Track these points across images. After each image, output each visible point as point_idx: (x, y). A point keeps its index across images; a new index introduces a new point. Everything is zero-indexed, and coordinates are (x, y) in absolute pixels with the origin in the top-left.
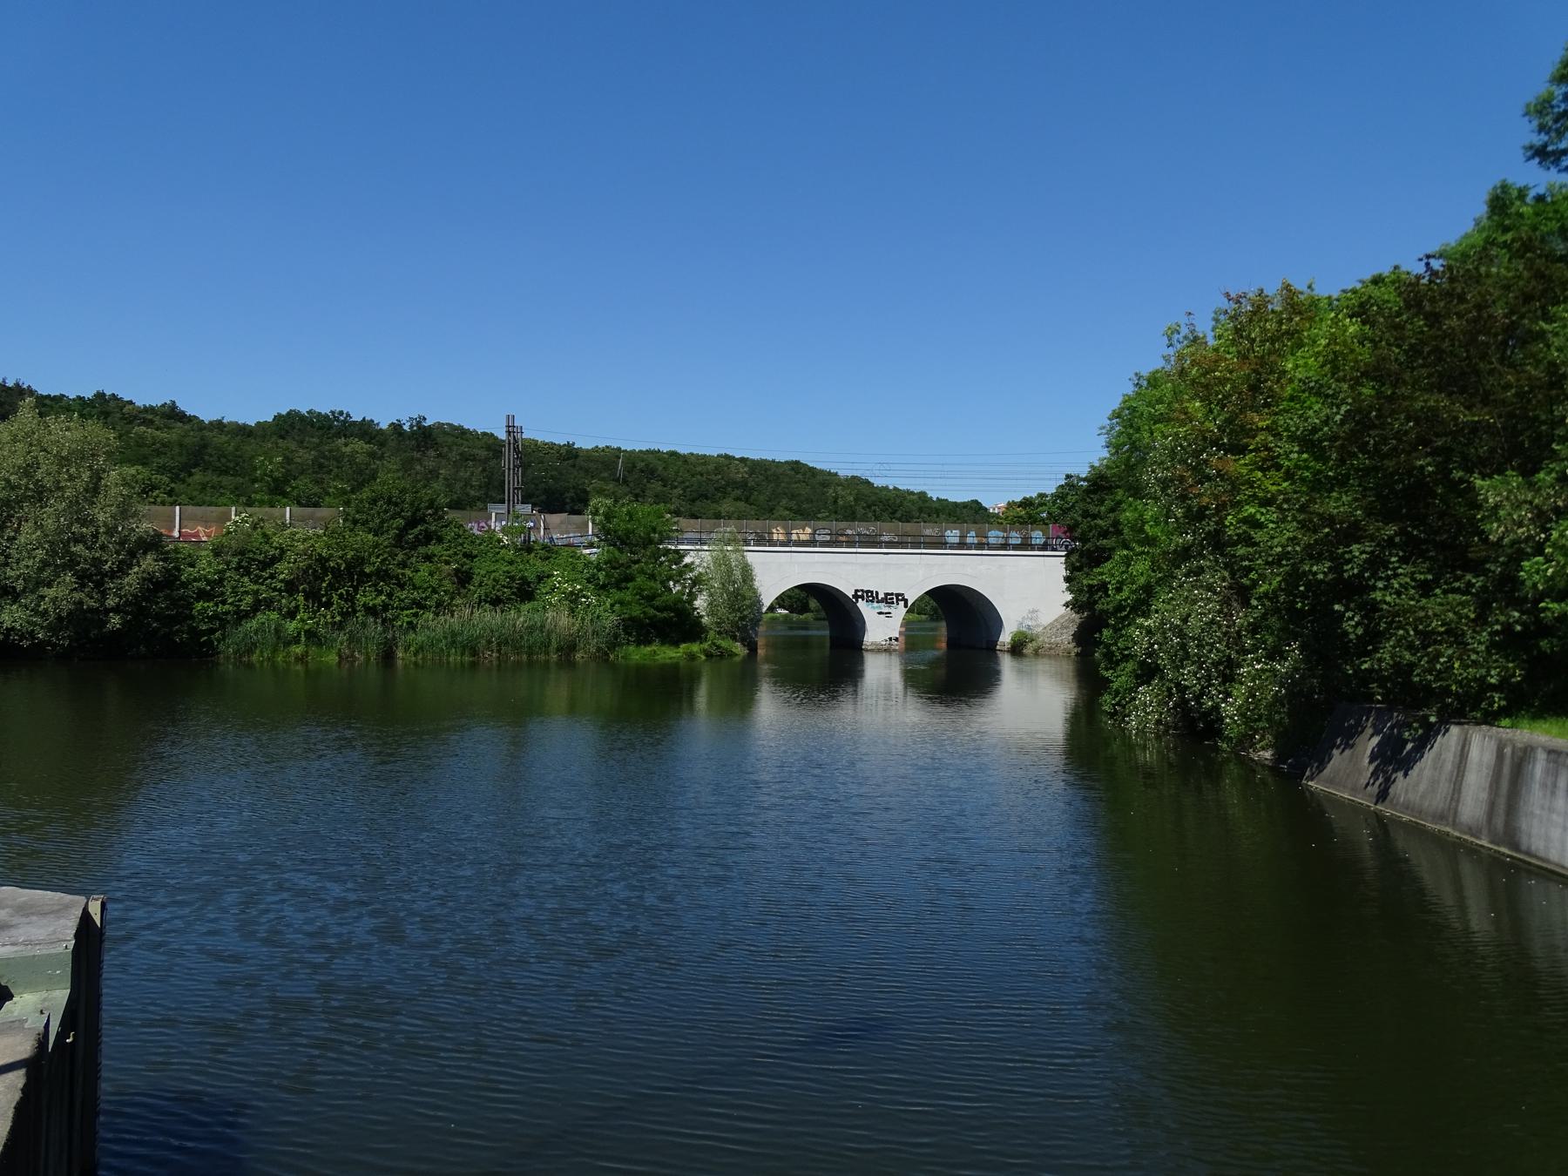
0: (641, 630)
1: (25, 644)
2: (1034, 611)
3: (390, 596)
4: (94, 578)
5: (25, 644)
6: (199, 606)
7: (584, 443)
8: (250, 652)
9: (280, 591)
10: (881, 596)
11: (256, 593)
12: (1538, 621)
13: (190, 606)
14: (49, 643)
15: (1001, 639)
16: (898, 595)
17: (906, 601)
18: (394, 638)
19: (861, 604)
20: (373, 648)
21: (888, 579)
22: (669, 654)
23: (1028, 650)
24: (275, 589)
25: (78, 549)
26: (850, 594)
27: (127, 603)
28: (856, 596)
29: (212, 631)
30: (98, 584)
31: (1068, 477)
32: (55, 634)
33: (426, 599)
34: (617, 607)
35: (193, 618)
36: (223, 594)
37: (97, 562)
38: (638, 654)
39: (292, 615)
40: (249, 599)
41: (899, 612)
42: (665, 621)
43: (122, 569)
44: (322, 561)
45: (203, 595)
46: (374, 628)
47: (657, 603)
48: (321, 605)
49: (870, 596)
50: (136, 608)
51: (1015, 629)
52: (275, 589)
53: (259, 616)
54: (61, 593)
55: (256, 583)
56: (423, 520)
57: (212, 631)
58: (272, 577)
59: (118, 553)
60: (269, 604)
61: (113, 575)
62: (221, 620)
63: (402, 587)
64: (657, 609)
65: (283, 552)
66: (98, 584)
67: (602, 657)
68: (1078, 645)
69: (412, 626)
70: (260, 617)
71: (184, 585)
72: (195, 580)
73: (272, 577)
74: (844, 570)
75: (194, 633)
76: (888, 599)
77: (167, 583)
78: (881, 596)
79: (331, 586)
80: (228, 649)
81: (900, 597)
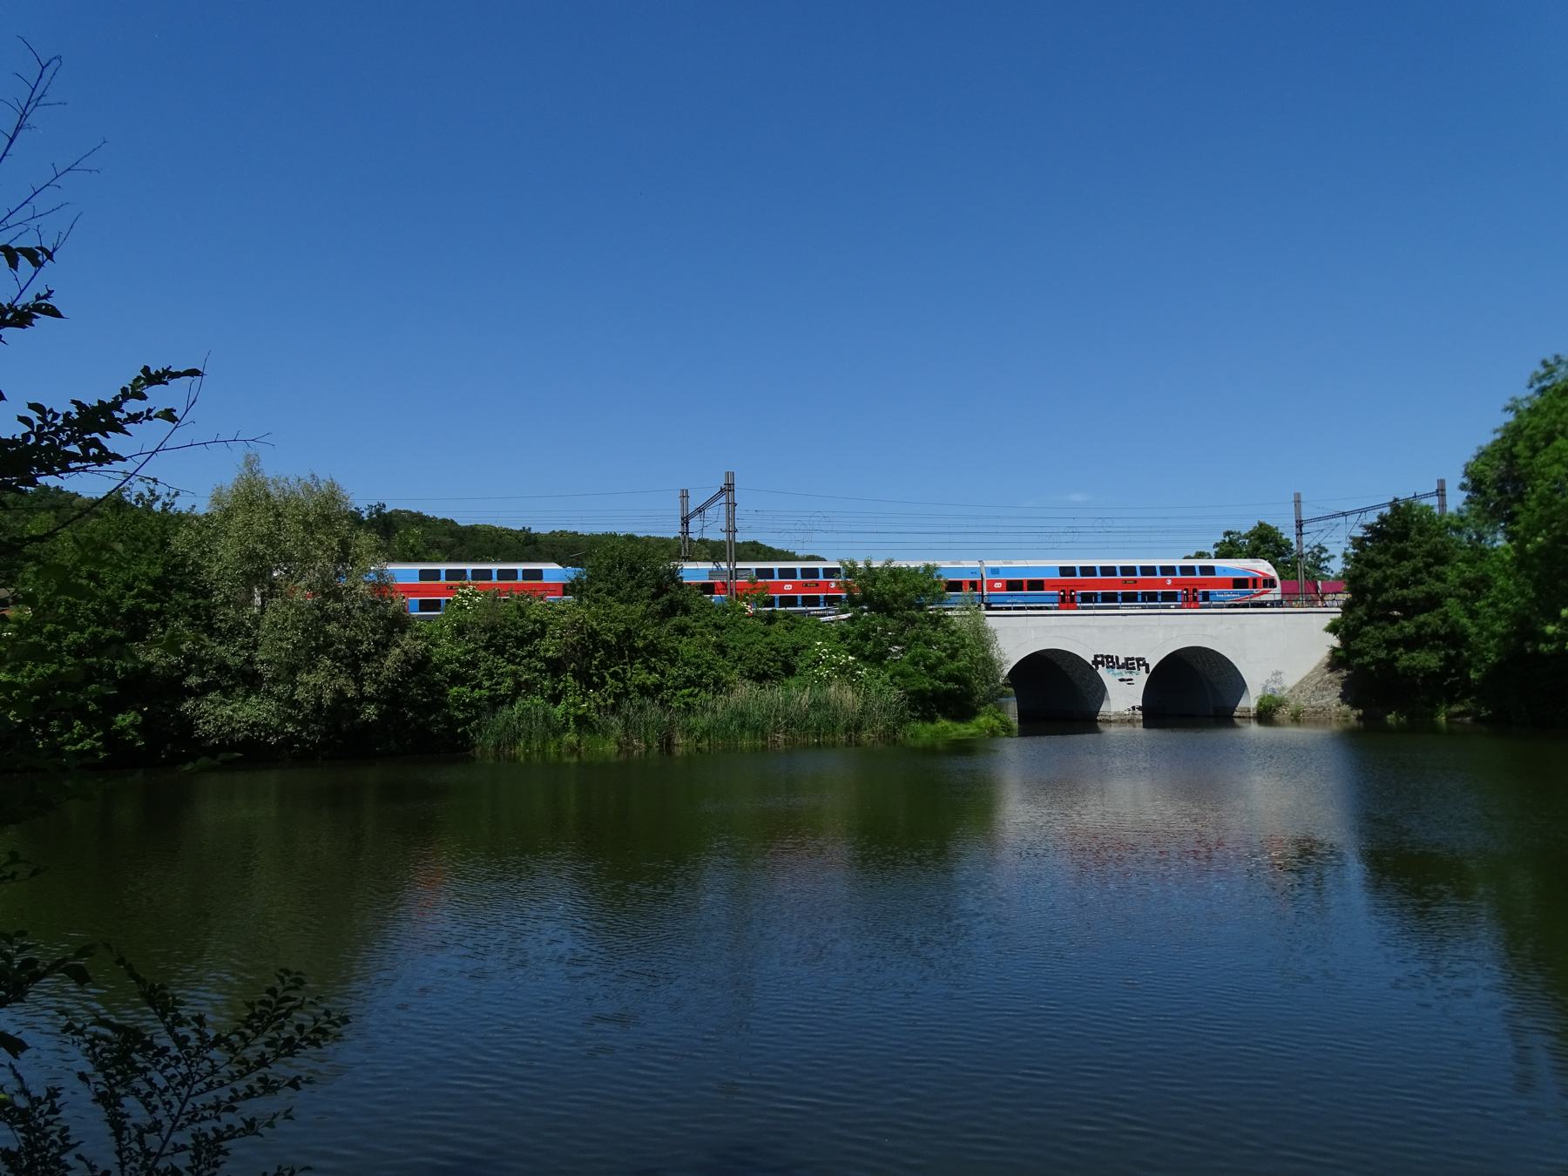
0: (927, 704)
1: (273, 740)
2: (1278, 673)
3: (662, 674)
4: (353, 662)
5: (273, 740)
6: (454, 691)
7: (463, 521)
8: (513, 743)
9: (540, 671)
10: (1122, 661)
11: (514, 674)
12: (362, 694)
13: (443, 693)
14: (299, 739)
15: (1242, 704)
16: (1138, 660)
17: (1147, 666)
18: (671, 722)
19: (1102, 671)
20: (653, 734)
21: (1126, 644)
22: (948, 728)
23: (1284, 713)
24: (536, 670)
25: (332, 628)
26: (1090, 660)
27: (386, 690)
28: (1096, 662)
29: (467, 721)
30: (355, 667)
31: (1261, 525)
32: (305, 727)
33: (701, 677)
34: (897, 679)
35: (446, 705)
36: (475, 677)
37: (353, 643)
38: (925, 732)
39: (555, 699)
40: (509, 682)
41: (1141, 678)
42: (948, 693)
43: (383, 646)
44: (593, 634)
45: (456, 679)
46: (653, 711)
47: (942, 671)
48: (591, 685)
49: (1110, 661)
50: (392, 698)
51: (1259, 693)
52: (536, 670)
53: (520, 701)
54: (320, 682)
55: (509, 661)
56: (667, 591)
57: (467, 721)
58: (530, 655)
59: (374, 631)
60: (529, 686)
61: (368, 657)
62: (476, 707)
63: (672, 662)
64: (939, 678)
65: (544, 625)
66: (355, 667)
67: (889, 736)
68: (1354, 706)
69: (689, 708)
70: (521, 704)
71: (438, 668)
72: (448, 661)
73: (530, 655)
74: (1080, 634)
75: (450, 720)
76: (1130, 664)
77: (419, 666)
78: (1122, 661)
79: (603, 665)
80: (485, 742)
81: (1141, 662)
